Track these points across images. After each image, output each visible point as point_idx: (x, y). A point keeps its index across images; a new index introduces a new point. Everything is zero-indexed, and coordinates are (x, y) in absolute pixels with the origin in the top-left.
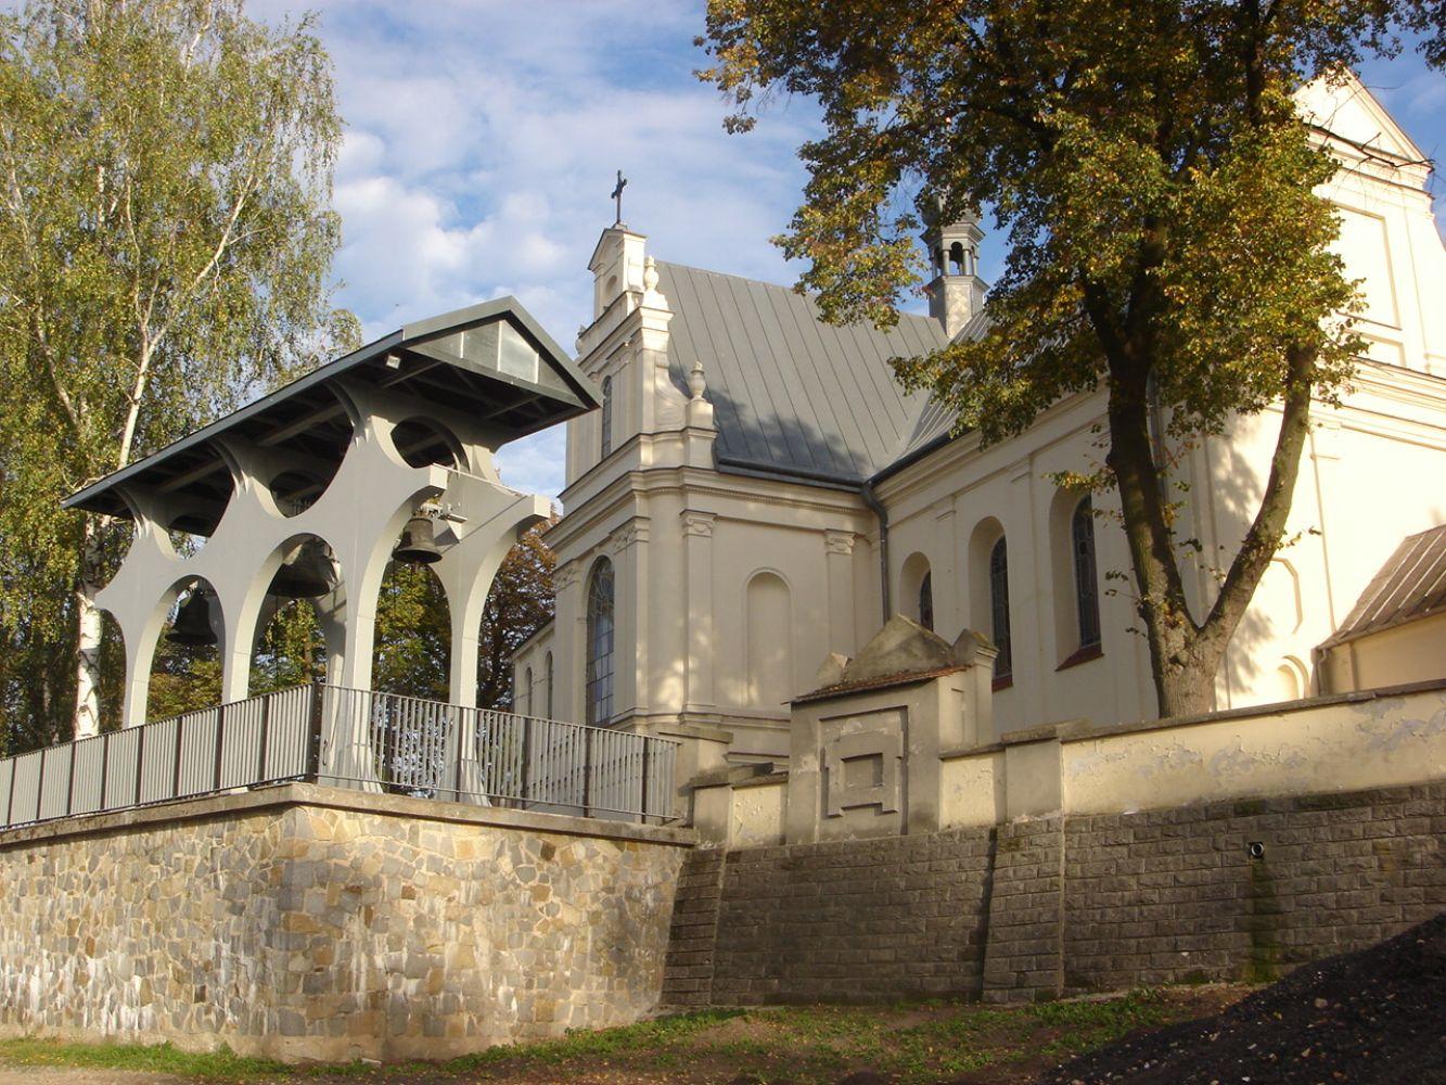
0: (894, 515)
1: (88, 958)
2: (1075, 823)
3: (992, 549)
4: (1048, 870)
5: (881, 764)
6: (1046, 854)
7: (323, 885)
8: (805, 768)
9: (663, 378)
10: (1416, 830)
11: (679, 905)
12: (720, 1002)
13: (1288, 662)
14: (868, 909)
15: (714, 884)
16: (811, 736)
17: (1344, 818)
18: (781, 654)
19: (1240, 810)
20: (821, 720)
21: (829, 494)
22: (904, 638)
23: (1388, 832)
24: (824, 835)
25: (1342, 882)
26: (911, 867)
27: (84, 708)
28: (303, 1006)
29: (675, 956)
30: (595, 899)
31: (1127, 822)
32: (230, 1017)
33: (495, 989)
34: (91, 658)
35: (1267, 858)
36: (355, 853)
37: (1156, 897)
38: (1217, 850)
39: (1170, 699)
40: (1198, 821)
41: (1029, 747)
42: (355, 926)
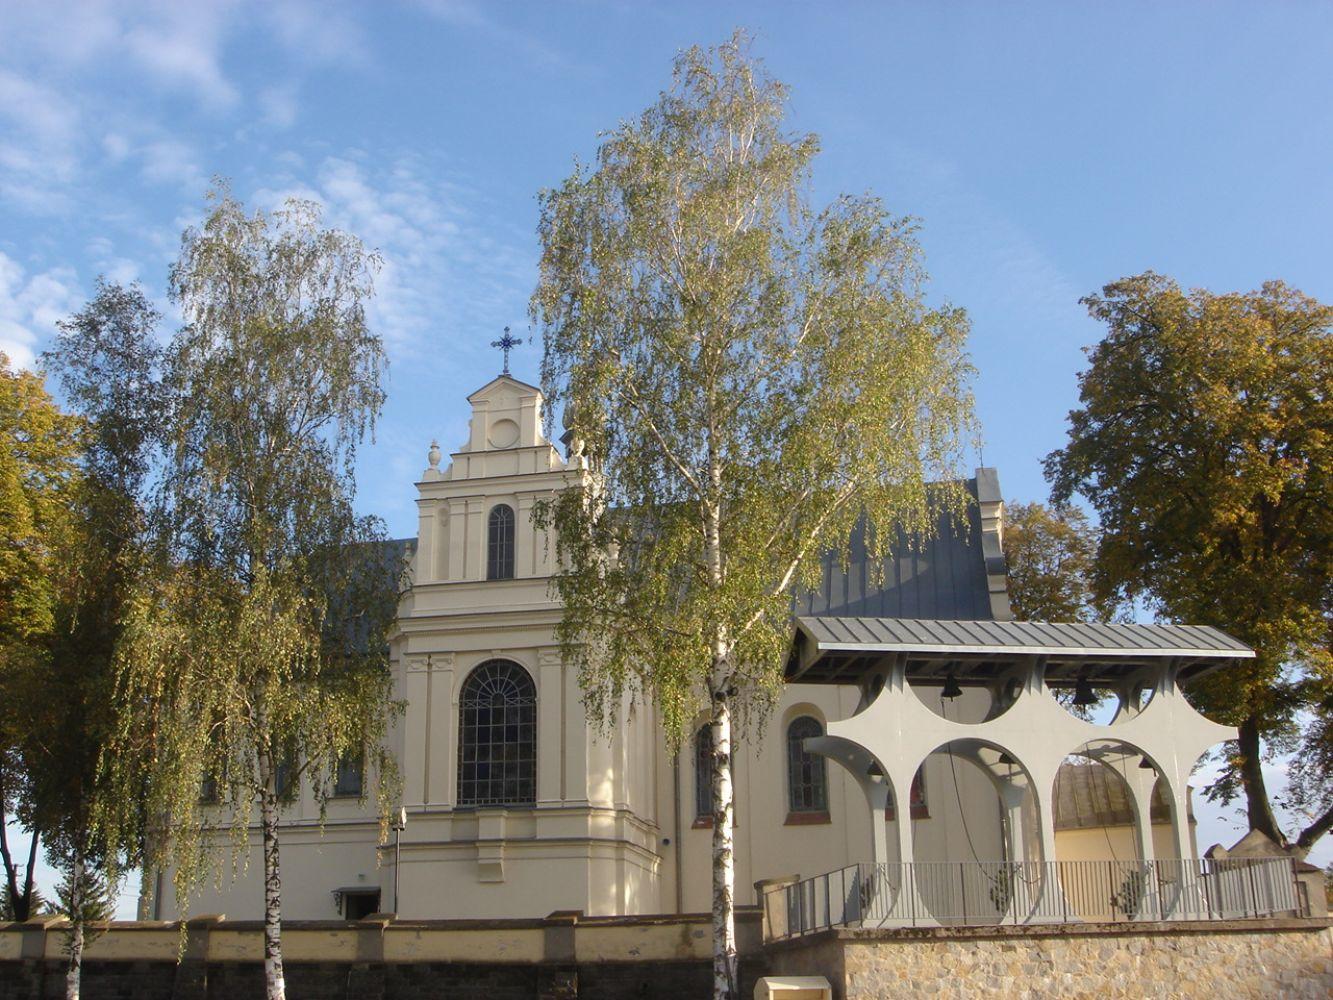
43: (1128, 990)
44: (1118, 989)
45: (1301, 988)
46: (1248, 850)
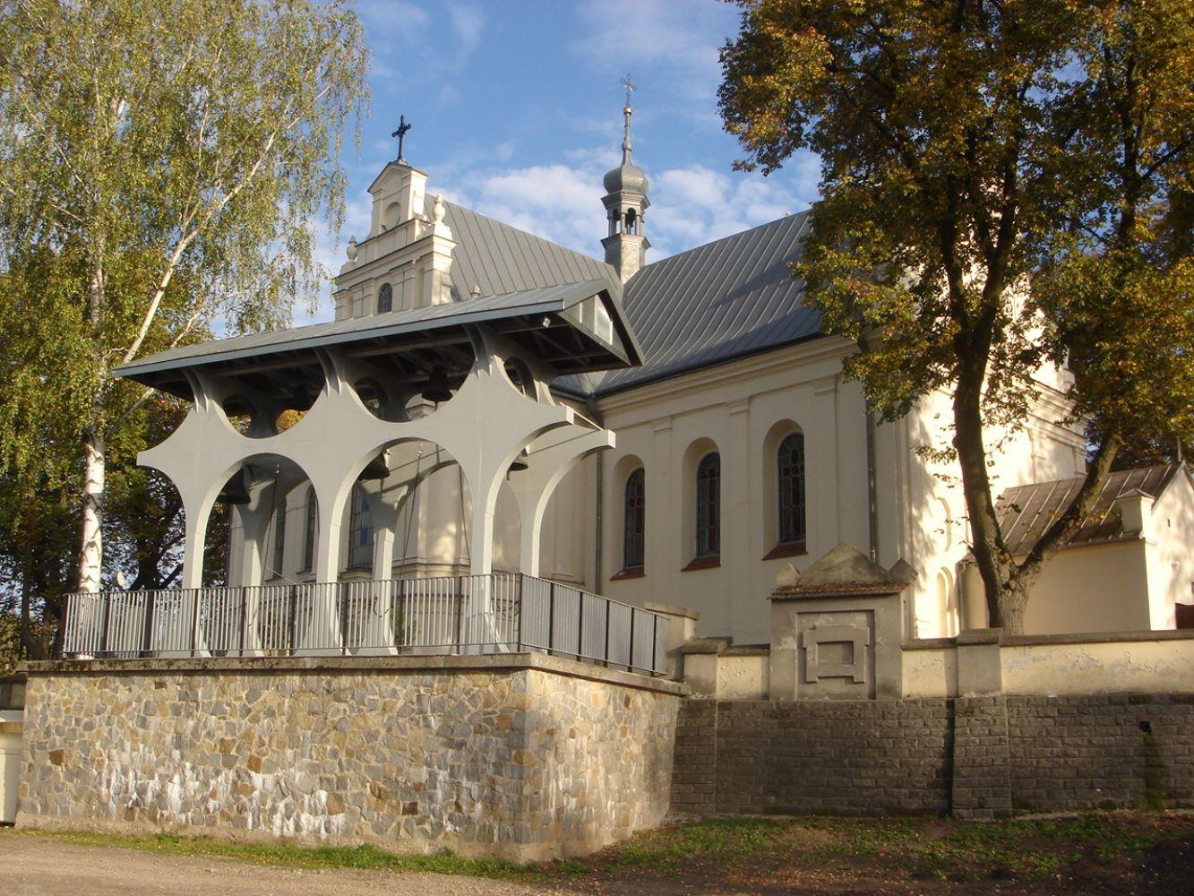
1: (253, 774)
2: (1012, 700)
4: (998, 731)
5: (853, 648)
8: (785, 647)
9: (445, 294)
12: (724, 811)
13: (942, 572)
14: (850, 750)
16: (790, 624)
20: (799, 613)
24: (802, 695)
27: (92, 544)
31: (1052, 702)
32: (449, 827)
34: (98, 501)
37: (1076, 753)
38: (1118, 724)
39: (1002, 613)
41: (976, 647)
42: (551, 759)
43: (271, 738)
44: (260, 737)
45: (475, 748)
46: (827, 570)
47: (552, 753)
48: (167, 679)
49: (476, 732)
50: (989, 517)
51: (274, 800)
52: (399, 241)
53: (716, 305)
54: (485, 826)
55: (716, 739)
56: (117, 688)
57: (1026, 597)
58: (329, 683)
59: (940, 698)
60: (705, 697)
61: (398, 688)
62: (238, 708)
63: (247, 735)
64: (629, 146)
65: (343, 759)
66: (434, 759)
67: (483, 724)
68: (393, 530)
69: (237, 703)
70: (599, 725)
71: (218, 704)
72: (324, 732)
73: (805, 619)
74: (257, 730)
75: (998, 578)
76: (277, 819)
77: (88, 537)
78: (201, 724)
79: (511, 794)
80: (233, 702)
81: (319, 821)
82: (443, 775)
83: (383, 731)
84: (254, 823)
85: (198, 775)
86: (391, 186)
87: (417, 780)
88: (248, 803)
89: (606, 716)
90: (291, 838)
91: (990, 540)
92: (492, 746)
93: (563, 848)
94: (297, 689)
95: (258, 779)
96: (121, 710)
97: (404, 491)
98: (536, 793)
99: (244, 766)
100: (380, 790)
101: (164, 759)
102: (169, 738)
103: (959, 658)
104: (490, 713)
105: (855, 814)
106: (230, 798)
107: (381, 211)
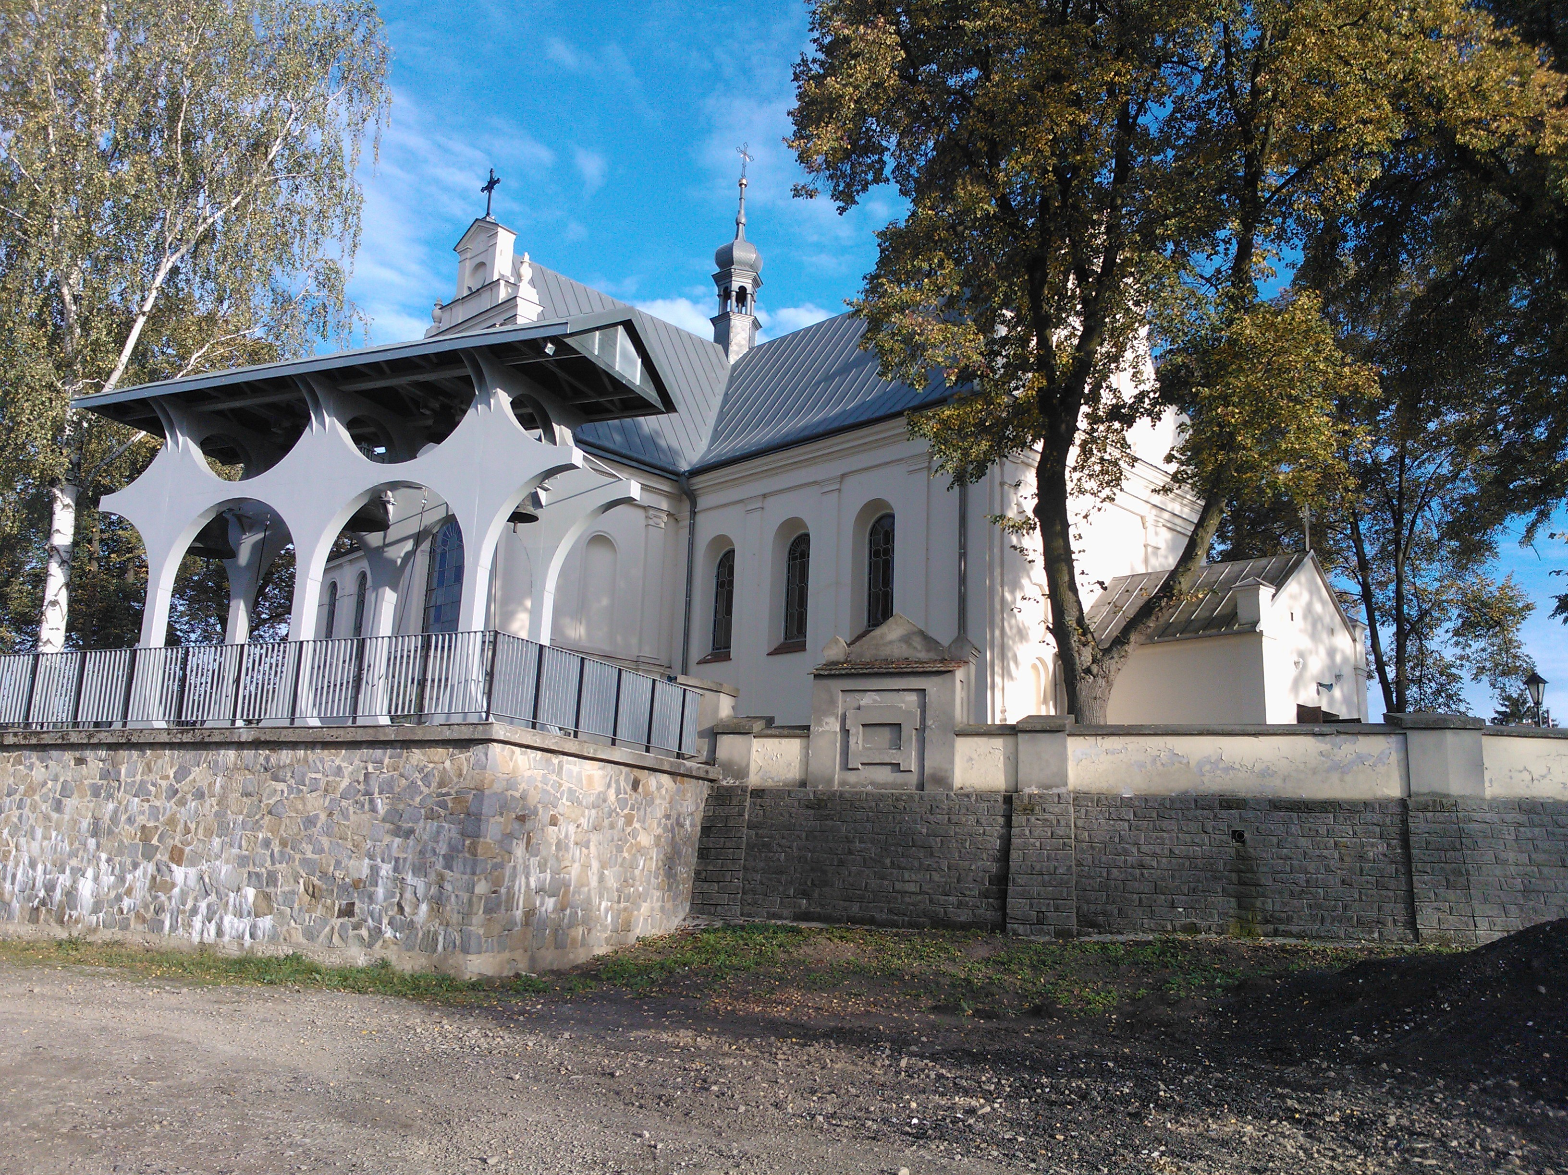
0: (703, 502)
1: (174, 867)
2: (1079, 798)
3: (790, 543)
4: (1061, 833)
6: (1058, 821)
7: (501, 814)
8: (827, 728)
10: (1369, 834)
11: (706, 830)
12: (749, 915)
15: (741, 815)
16: (832, 702)
17: (1311, 820)
18: (605, 602)
19: (1224, 804)
21: (655, 478)
22: (905, 632)
23: (1345, 832)
24: (843, 783)
25: (1311, 868)
26: (931, 818)
27: (54, 603)
28: (482, 926)
29: (704, 874)
30: (659, 824)
31: (1127, 803)
32: (389, 933)
33: (600, 904)
34: (63, 554)
35: (1249, 842)
36: (523, 786)
37: (1155, 864)
40: (1188, 809)
42: (519, 851)
43: (198, 823)
47: (522, 845)
48: (89, 754)
49: (427, 818)
50: (1070, 594)
51: (196, 899)
52: (484, 302)
53: (818, 383)
54: (429, 932)
55: (745, 830)
56: (32, 765)
57: (1109, 684)
58: (267, 759)
59: (997, 792)
60: (737, 783)
61: (344, 765)
62: (164, 788)
63: (172, 821)
64: (743, 221)
65: (276, 850)
66: (378, 850)
67: (435, 808)
68: (394, 588)
69: (164, 783)
70: (593, 811)
71: (143, 783)
72: (257, 817)
73: (849, 697)
74: (183, 814)
75: (1078, 662)
76: (197, 921)
77: (49, 596)
78: (122, 808)
79: (460, 893)
80: (159, 781)
81: (243, 925)
82: (386, 870)
83: (323, 816)
84: (171, 926)
85: (113, 868)
86: (476, 245)
87: (356, 876)
88: (167, 903)
89: (605, 801)
90: (210, 945)
91: (1071, 620)
92: (444, 836)
93: (533, 959)
94: (231, 766)
95: (179, 873)
96: (34, 792)
97: (409, 545)
98: (494, 892)
99: (166, 858)
100: (314, 886)
101: (78, 850)
102: (85, 824)
103: (1020, 748)
104: (444, 795)
105: (894, 925)
106: (148, 895)
107: (468, 271)
